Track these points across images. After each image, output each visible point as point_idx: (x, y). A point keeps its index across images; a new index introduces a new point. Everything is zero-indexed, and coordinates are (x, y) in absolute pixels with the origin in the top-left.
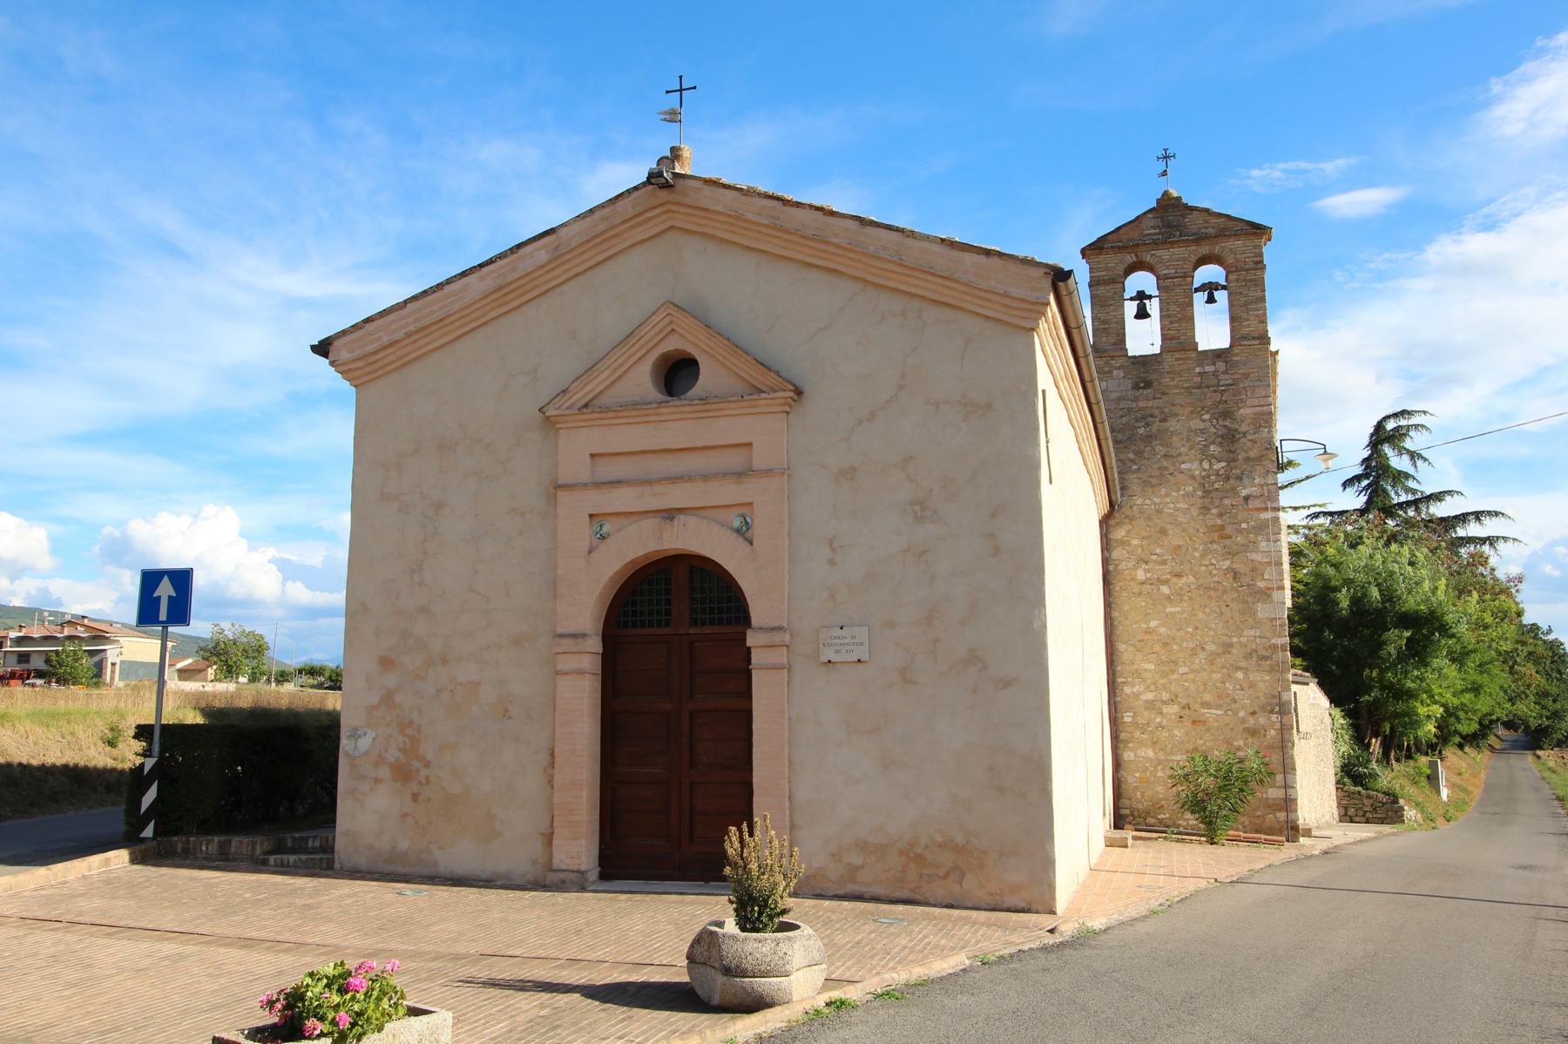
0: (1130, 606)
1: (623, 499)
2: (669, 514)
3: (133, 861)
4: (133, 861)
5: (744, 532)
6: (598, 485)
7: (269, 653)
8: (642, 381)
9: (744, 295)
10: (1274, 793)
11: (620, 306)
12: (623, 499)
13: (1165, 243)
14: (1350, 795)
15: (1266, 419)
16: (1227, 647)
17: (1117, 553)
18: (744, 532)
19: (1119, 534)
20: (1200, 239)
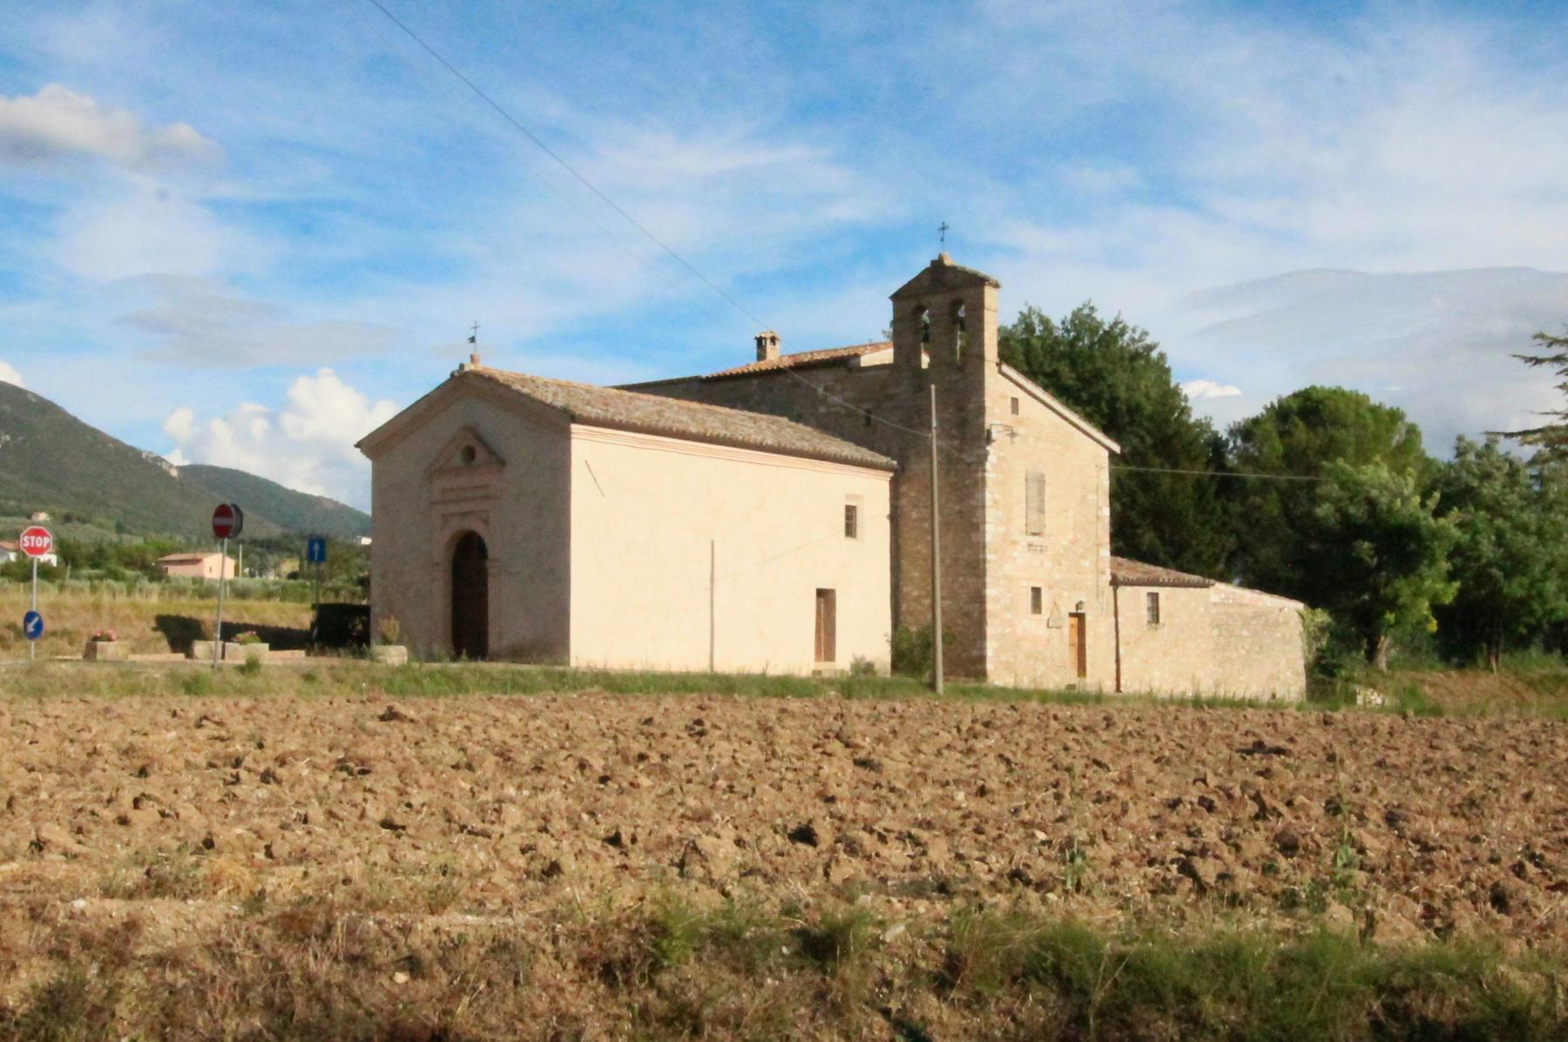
0: (908, 536)
1: (452, 508)
2: (464, 515)
3: (272, 648)
4: (272, 648)
5: (486, 522)
6: (444, 503)
7: (877, 667)
8: (457, 460)
9: (492, 422)
10: (975, 653)
11: (447, 426)
12: (452, 508)
13: (932, 292)
14: (1317, 682)
15: (981, 411)
16: (956, 561)
17: (903, 501)
18: (486, 522)
19: (904, 488)
20: (952, 289)
